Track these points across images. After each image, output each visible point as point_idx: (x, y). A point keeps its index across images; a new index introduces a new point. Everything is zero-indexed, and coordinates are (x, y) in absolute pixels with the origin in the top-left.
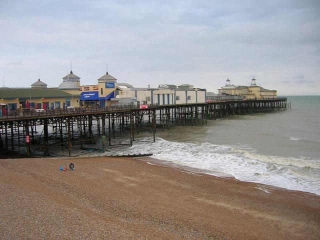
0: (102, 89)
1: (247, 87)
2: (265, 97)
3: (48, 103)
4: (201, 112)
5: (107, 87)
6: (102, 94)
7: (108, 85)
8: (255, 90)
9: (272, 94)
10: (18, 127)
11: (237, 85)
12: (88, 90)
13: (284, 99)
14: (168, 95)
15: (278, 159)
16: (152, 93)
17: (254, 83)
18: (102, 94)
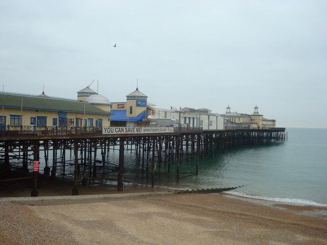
0: (131, 107)
1: (249, 115)
2: (267, 126)
3: (45, 119)
4: (29, 153)
5: (138, 105)
6: (131, 112)
7: (140, 103)
8: (257, 120)
9: (269, 123)
10: (131, 144)
11: (240, 112)
12: (123, 107)
13: (283, 130)
14: (193, 118)
15: (300, 202)
16: (180, 116)
17: (228, 111)
18: (131, 112)
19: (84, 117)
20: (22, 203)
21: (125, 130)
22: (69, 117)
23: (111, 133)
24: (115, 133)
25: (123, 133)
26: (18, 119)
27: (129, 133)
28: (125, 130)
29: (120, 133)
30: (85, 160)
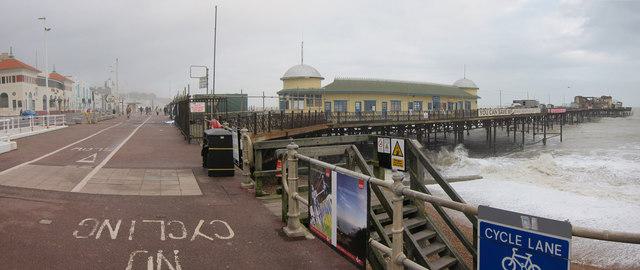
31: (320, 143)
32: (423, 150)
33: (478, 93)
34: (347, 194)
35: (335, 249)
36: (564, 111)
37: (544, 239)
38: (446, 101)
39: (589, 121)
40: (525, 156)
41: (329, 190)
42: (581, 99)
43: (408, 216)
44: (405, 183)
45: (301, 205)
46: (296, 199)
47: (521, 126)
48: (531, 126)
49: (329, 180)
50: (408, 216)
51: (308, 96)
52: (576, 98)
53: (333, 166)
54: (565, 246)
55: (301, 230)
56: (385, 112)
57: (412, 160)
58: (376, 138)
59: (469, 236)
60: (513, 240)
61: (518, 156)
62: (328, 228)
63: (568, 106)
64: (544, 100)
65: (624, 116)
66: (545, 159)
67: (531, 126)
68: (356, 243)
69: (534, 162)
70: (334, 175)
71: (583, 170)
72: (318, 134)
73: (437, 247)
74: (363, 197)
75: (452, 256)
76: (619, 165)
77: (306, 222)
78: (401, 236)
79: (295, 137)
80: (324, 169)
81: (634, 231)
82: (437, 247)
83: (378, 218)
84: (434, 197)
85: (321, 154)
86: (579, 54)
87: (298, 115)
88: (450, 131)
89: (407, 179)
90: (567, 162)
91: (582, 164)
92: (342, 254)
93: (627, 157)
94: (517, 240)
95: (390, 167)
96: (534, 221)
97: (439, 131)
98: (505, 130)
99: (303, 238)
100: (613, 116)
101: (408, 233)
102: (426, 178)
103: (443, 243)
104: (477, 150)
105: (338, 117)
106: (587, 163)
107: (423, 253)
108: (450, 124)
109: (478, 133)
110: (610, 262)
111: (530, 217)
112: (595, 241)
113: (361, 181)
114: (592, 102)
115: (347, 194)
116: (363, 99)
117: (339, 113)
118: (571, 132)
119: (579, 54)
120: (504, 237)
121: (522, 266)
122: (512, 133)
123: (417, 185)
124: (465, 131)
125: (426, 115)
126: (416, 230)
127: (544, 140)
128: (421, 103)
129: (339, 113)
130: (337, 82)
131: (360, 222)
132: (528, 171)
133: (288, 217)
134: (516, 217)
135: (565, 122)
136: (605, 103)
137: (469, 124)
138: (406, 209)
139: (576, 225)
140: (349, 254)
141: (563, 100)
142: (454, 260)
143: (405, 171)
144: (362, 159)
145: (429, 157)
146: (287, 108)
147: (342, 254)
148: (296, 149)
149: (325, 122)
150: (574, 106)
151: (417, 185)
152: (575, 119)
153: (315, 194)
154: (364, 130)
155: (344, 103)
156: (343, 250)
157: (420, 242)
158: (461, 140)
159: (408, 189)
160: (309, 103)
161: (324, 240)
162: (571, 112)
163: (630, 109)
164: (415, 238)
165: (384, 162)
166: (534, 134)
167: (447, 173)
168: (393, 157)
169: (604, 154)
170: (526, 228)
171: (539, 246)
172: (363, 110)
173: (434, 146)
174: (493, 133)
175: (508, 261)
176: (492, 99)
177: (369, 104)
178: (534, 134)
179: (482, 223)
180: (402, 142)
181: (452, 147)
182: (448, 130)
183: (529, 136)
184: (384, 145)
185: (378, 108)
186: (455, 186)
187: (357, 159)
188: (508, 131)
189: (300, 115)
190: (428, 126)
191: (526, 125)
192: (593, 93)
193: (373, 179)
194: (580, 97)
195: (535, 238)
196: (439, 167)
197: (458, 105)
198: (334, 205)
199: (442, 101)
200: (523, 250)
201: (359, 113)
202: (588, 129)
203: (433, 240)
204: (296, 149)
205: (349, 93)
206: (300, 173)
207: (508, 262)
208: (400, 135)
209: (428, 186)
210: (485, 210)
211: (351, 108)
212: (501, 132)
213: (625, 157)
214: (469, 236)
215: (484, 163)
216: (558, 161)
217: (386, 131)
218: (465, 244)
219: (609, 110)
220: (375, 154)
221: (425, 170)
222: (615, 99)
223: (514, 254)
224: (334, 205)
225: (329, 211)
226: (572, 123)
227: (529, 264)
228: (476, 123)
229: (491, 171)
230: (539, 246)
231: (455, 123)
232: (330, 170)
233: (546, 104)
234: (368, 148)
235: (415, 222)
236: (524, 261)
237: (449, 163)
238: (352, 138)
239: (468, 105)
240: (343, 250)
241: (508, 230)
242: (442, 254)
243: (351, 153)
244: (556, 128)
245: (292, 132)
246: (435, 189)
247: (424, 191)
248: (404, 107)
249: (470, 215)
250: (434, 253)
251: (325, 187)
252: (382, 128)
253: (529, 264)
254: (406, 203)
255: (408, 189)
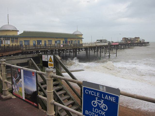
19: (74, 40)
20: (8, 57)
21: (90, 45)
22: (68, 40)
23: (86, 46)
24: (87, 46)
25: (90, 46)
26: (28, 42)
27: (92, 45)
28: (90, 45)
29: (89, 46)
30: (16, 48)
31: (17, 58)
32: (61, 59)
33: (83, 37)
34: (28, 78)
35: (23, 100)
36: (118, 44)
37: (108, 95)
38: (70, 40)
39: (129, 48)
40: (101, 62)
41: (20, 77)
42: (125, 39)
43: (55, 85)
44: (54, 73)
45: (9, 85)
46: (6, 83)
47: (100, 50)
48: (104, 50)
49: (20, 73)
50: (55, 85)
51: (12, 38)
52: (123, 39)
53: (22, 67)
54: (117, 99)
55: (10, 95)
56: (45, 45)
57: (56, 63)
58: (42, 55)
59: (79, 92)
60: (96, 94)
61: (98, 62)
62: (21, 93)
63: (120, 42)
64: (109, 40)
65: (145, 46)
66: (109, 63)
67: (104, 50)
68: (33, 98)
69: (105, 64)
70: (22, 71)
71: (125, 68)
72: (17, 54)
73: (67, 97)
74: (34, 79)
75: (73, 100)
76: (142, 67)
77: (11, 91)
78: (52, 93)
79: (14, 55)
80: (18, 69)
81: (153, 97)
82: (67, 97)
83: (42, 87)
84: (65, 78)
85: (17, 63)
86: (125, 20)
87: (7, 46)
88: (71, 52)
89: (55, 71)
90: (119, 65)
91: (125, 66)
92: (28, 102)
93: (146, 64)
94: (98, 95)
95: (48, 67)
96: (104, 88)
97: (67, 52)
98: (93, 52)
99: (10, 98)
100: (140, 46)
101: (55, 92)
102: (62, 71)
103: (69, 95)
104: (82, 59)
105: (26, 47)
106: (128, 65)
107: (61, 99)
108: (70, 49)
109: (82, 53)
110: (137, 107)
111: (103, 86)
112: (130, 98)
113: (33, 73)
114: (131, 40)
115: (28, 78)
116: (36, 40)
117: (26, 45)
118: (120, 53)
119: (125, 20)
120: (93, 93)
121: (99, 104)
122: (96, 53)
123: (58, 73)
124: (78, 52)
125: (62, 45)
126: (58, 91)
127: (109, 56)
128: (60, 41)
129: (26, 45)
130: (25, 33)
131: (34, 89)
132: (102, 68)
133: (3, 91)
134: (97, 86)
135: (118, 48)
136: (136, 40)
137: (79, 49)
138: (55, 83)
139: (121, 90)
140: (31, 102)
141: (117, 39)
142: (70, 96)
143: (54, 68)
144: (35, 64)
145: (63, 62)
146: (2, 43)
147: (28, 102)
148: (4, 61)
149: (20, 49)
150: (122, 42)
151: (58, 73)
152: (122, 47)
153: (14, 80)
154: (37, 52)
155: (28, 41)
156: (27, 100)
157: (60, 95)
158: (76, 56)
159: (55, 75)
160: (12, 41)
161: (20, 98)
162: (121, 44)
163: (148, 43)
164: (58, 94)
165: (45, 64)
166: (105, 53)
167: (70, 68)
168: (49, 63)
169: (135, 62)
170: (101, 90)
171: (106, 97)
172: (36, 44)
173: (65, 58)
174: (88, 53)
175: (94, 102)
176: (88, 40)
177: (39, 42)
178: (105, 53)
179: (84, 88)
180: (52, 57)
181: (72, 58)
182: (71, 52)
183: (103, 54)
184: (45, 58)
185: (43, 43)
186: (74, 74)
187: (33, 64)
188: (94, 52)
189: (8, 47)
190: (63, 50)
191: (102, 50)
192: (131, 36)
193: (40, 72)
194: (125, 38)
195: (105, 94)
196: (68, 66)
197: (75, 42)
198: (23, 83)
199: (68, 40)
200: (100, 99)
201: (35, 45)
202: (128, 51)
203: (65, 94)
204: (4, 61)
205: (30, 37)
206: (7, 72)
207: (94, 102)
208: (52, 54)
209: (63, 74)
210: (85, 83)
211: (31, 43)
212: (92, 53)
213: (145, 64)
214: (79, 92)
215: (85, 64)
216: (115, 64)
217: (46, 52)
218: (78, 95)
219: (138, 43)
220: (41, 62)
221: (62, 68)
222: (141, 38)
223: (96, 100)
224: (23, 83)
225: (21, 86)
226: (121, 49)
227: (102, 104)
228: (82, 49)
229: (88, 68)
230: (106, 97)
231: (74, 49)
232: (20, 69)
233: (110, 41)
234: (38, 59)
235: (58, 87)
236: (100, 103)
237: (71, 65)
238: (31, 56)
239: (79, 42)
240: (27, 100)
241: (94, 91)
242: (69, 99)
243: (30, 62)
244: (114, 51)
245: (4, 54)
246: (66, 75)
247: (62, 75)
248: (53, 43)
249: (80, 84)
250: (66, 99)
251: (18, 76)
252: (44, 51)
253: (102, 104)
254: (54, 80)
255: (55, 75)
